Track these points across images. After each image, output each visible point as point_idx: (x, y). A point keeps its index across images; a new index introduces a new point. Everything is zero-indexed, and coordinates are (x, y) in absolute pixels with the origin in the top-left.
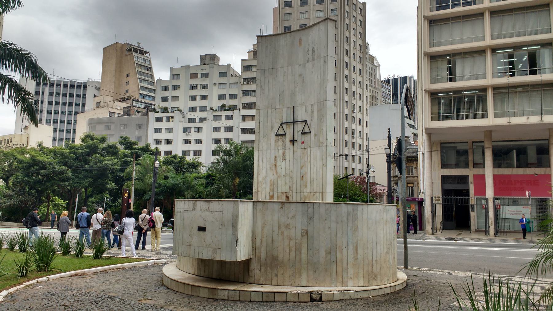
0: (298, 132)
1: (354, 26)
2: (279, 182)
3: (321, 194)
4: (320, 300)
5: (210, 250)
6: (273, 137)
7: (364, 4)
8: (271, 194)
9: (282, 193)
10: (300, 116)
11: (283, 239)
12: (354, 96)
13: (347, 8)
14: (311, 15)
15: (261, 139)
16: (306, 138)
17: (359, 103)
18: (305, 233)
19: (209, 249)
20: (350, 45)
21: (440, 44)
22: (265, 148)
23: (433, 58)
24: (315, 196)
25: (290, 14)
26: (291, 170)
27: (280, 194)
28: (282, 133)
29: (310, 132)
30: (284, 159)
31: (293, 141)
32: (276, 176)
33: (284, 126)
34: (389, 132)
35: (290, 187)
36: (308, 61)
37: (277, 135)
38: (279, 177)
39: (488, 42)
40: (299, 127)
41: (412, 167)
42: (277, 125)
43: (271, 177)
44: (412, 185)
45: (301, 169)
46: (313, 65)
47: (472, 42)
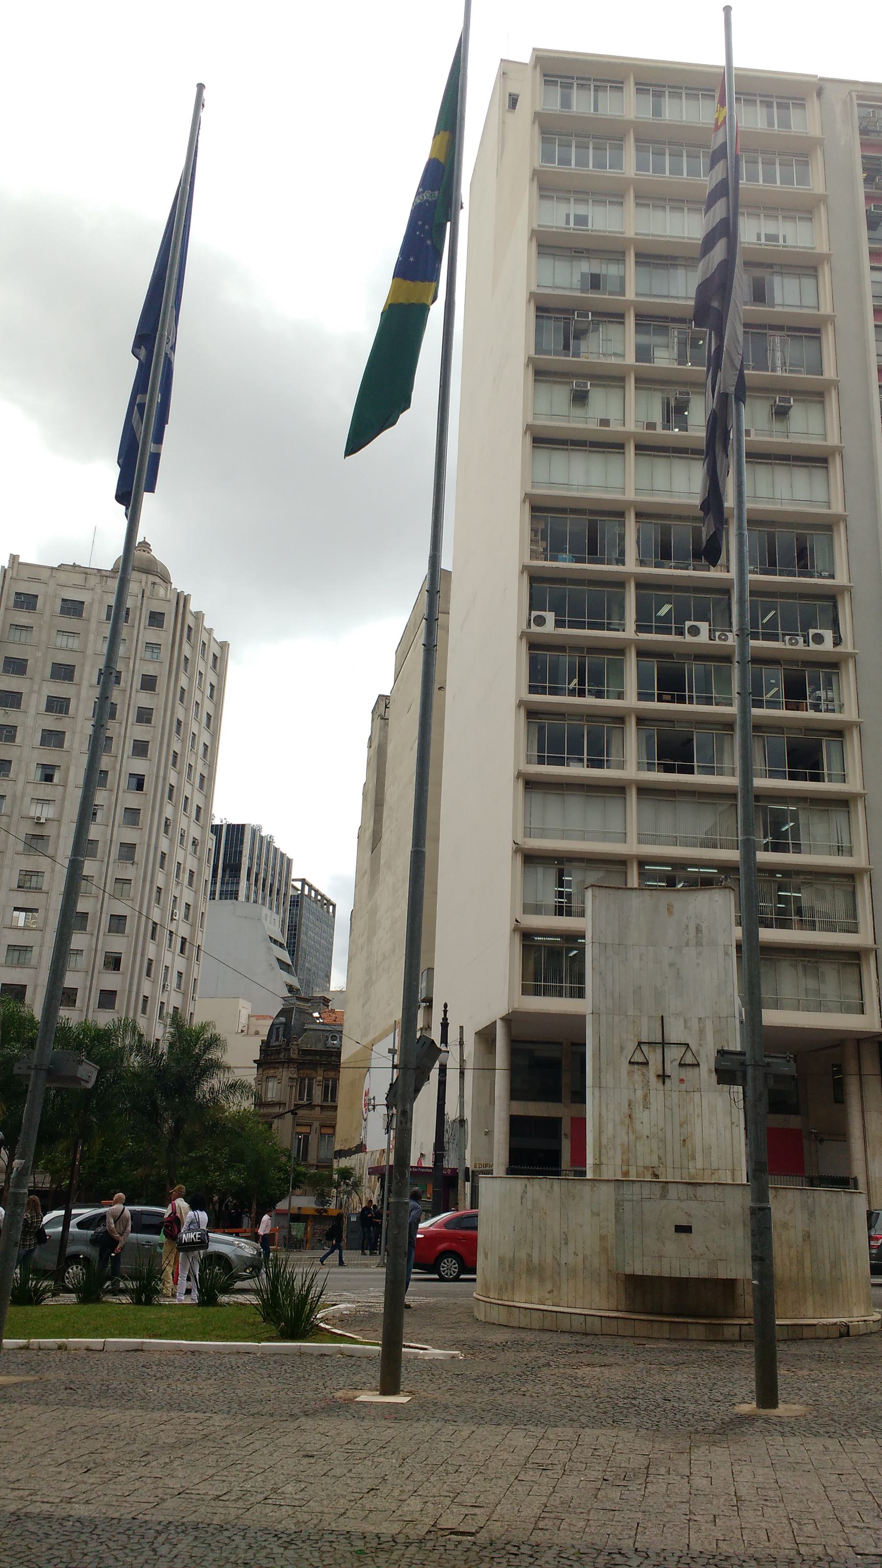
0: (672, 1062)
1: (197, 696)
2: (639, 1148)
4: (848, 1334)
5: (703, 1264)
6: (625, 1067)
7: (224, 646)
8: (625, 1168)
10: (675, 1033)
11: (781, 1246)
12: (178, 876)
13: (187, 650)
14: (90, 646)
15: (603, 1066)
16: (688, 1074)
17: (187, 896)
18: (807, 1236)
19: (701, 1261)
20: (183, 741)
21: (543, 833)
22: (611, 1086)
23: (531, 859)
25: (28, 628)
26: (660, 1127)
27: (641, 1169)
28: (641, 1059)
29: (698, 1065)
30: (646, 1107)
31: (663, 1077)
32: (632, 1137)
33: (645, 1048)
34: (445, 1012)
35: (660, 1158)
36: (687, 944)
37: (630, 1063)
38: (637, 1138)
39: (632, 847)
40: (673, 1054)
41: (311, 1080)
42: (631, 1046)
43: (622, 1138)
44: (305, 1130)
45: (681, 1126)
46: (700, 954)
47: (604, 840)
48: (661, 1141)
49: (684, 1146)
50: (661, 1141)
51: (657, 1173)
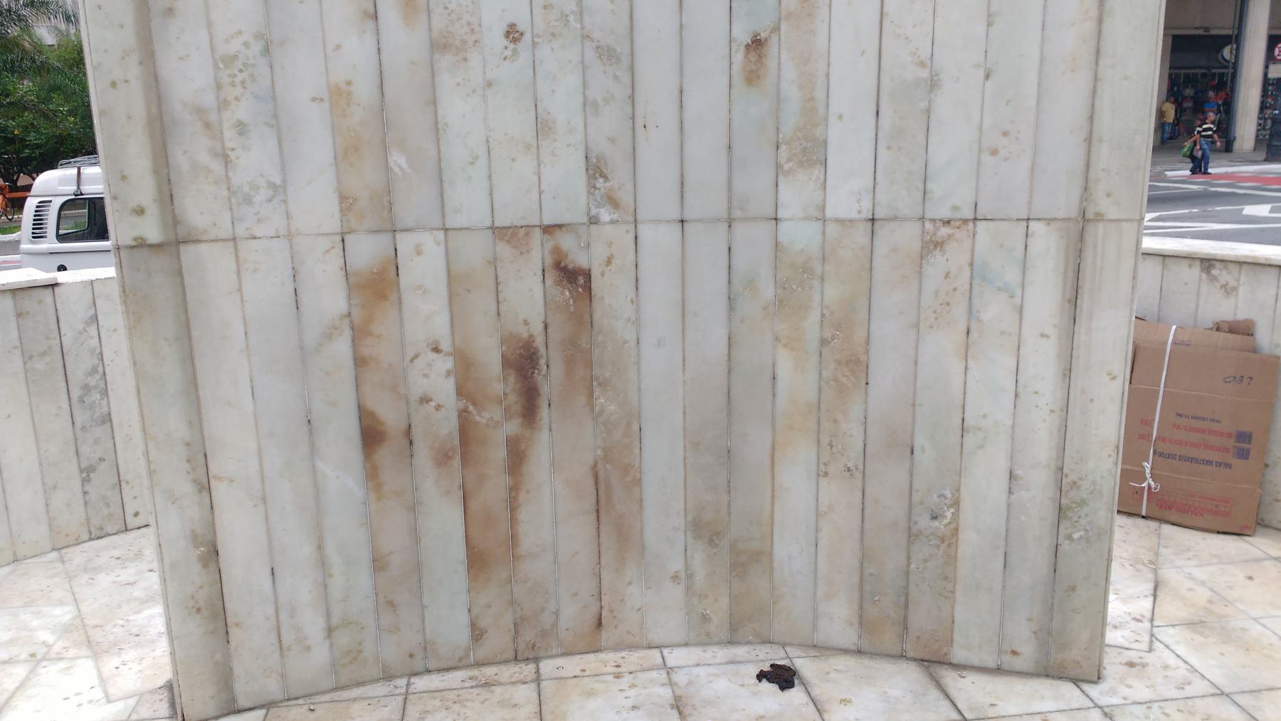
2: (457, 107)
3: (1047, 246)
8: (366, 250)
9: (502, 233)
24: (937, 265)
27: (475, 250)
32: (403, 40)
35: (595, 170)
38: (439, 45)
48: (607, 54)
49: (752, 77)
50: (607, 54)
51: (579, 259)
